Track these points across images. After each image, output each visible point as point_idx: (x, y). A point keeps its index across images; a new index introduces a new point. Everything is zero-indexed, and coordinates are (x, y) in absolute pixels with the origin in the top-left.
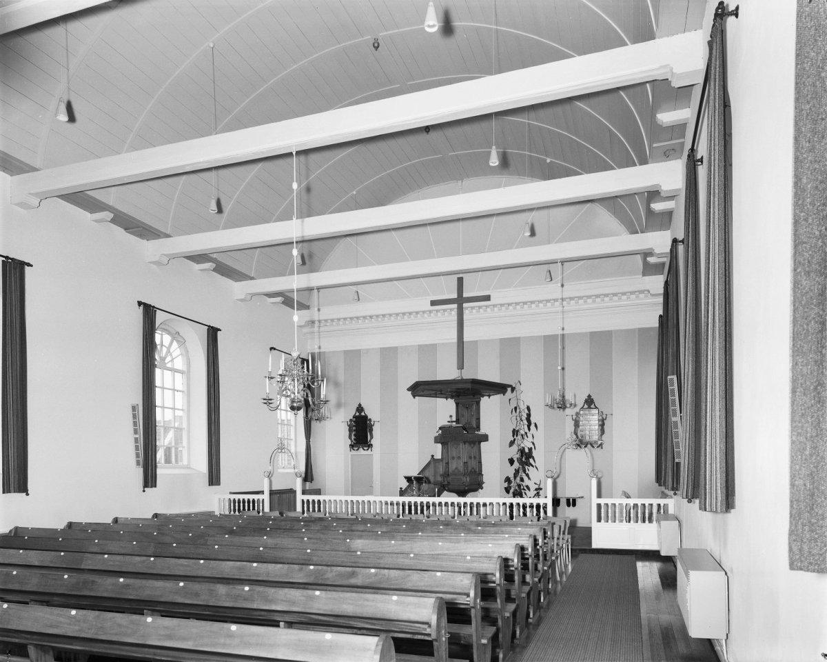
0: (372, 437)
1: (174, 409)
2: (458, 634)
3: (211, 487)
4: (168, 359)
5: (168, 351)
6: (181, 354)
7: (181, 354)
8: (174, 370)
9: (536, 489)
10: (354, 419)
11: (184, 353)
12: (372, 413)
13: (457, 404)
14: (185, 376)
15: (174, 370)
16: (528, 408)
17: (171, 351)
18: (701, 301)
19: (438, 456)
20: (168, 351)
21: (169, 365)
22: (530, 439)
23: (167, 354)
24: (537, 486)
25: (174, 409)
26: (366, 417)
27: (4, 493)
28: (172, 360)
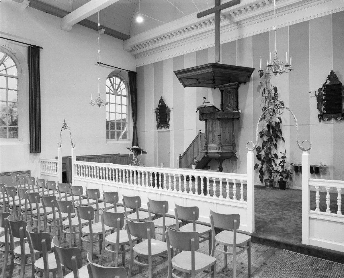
0: (169, 120)
1: (121, 113)
2: (319, 99)
3: (62, 158)
4: (119, 90)
5: (119, 87)
6: (126, 88)
7: (126, 88)
8: (121, 96)
9: (282, 157)
10: (158, 108)
11: (127, 87)
12: (169, 103)
13: (222, 91)
14: (128, 98)
15: (121, 96)
16: (275, 89)
17: (120, 86)
18: (212, 245)
19: (203, 131)
20: (119, 87)
21: (119, 93)
22: (277, 115)
23: (118, 88)
24: (282, 155)
25: (121, 113)
26: (165, 105)
27: (76, 156)
28: (121, 91)
